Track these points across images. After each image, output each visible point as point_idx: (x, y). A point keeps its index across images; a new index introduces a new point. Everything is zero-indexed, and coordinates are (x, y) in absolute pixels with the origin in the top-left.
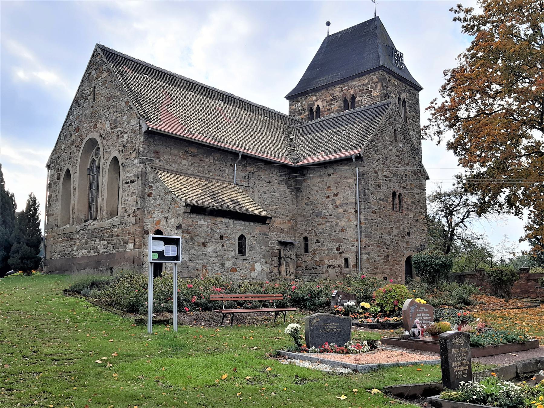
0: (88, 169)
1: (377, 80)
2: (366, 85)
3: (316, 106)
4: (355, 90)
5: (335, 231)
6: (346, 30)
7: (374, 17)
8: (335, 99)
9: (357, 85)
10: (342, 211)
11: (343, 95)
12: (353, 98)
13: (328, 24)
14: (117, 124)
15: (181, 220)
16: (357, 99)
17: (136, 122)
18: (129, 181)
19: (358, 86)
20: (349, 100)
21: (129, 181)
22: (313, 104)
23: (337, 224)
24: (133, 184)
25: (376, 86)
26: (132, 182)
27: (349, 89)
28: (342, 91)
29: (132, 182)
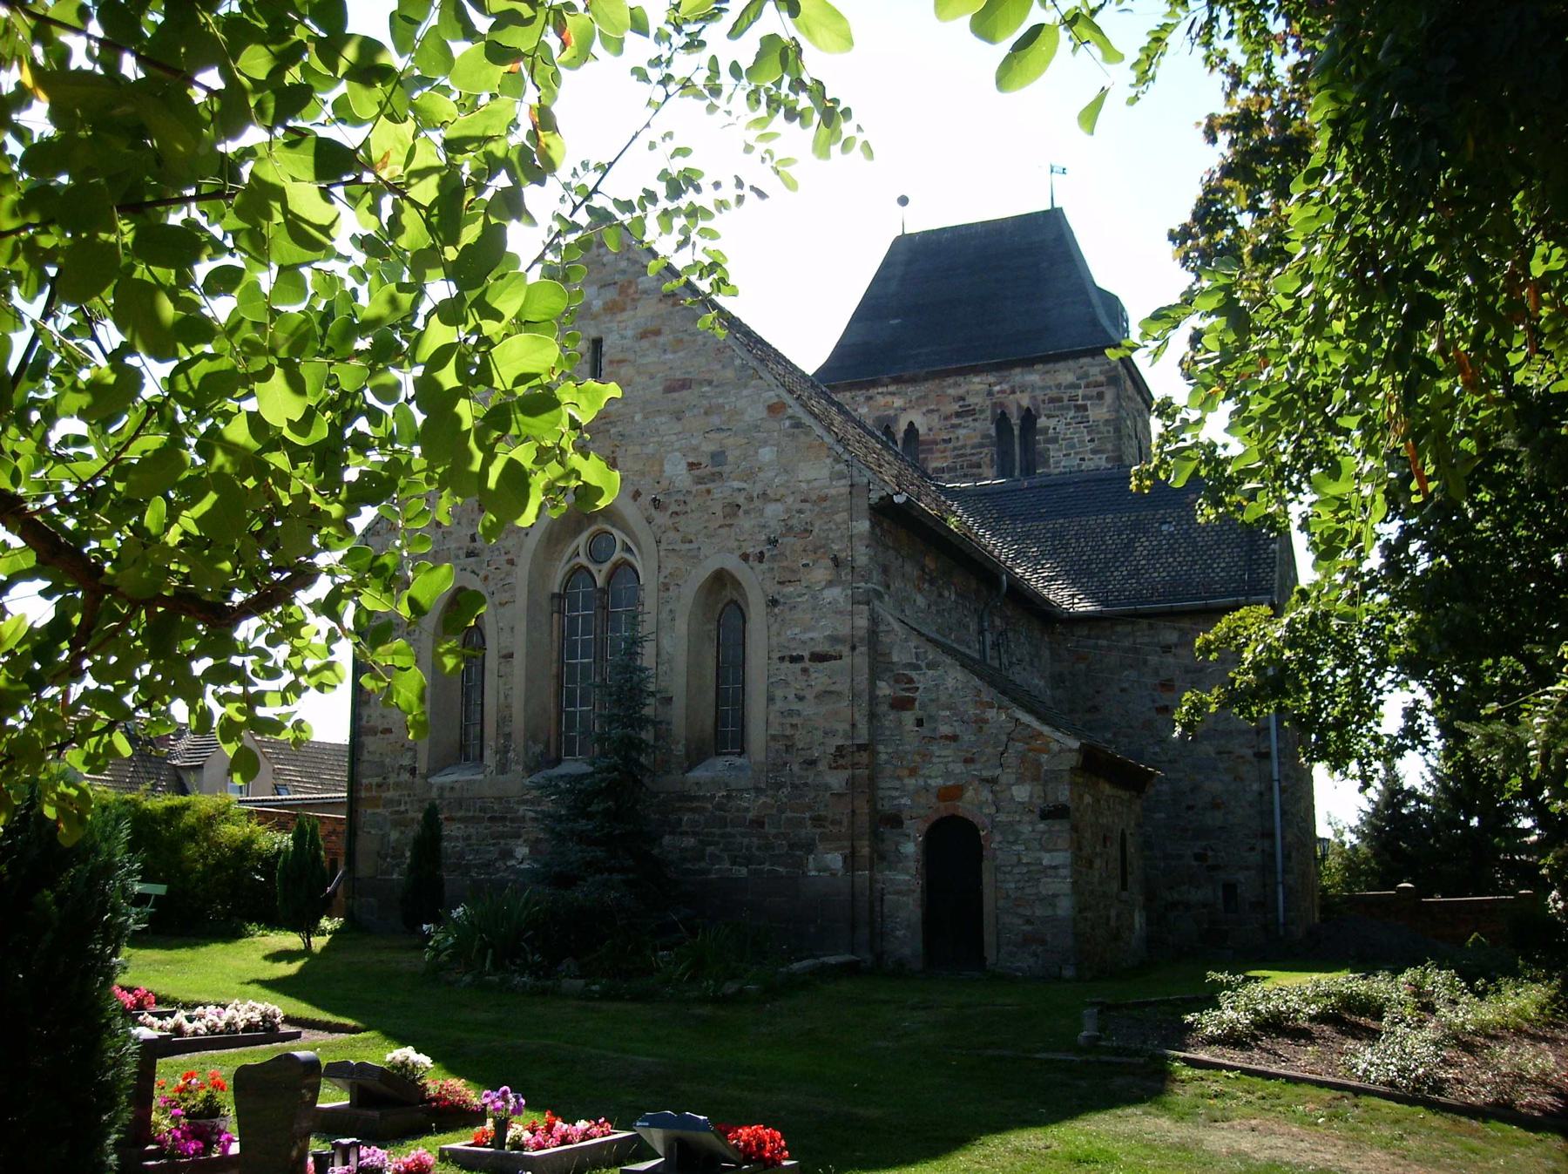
0: (554, 596)
1: (1102, 378)
2: (1067, 387)
3: (903, 426)
4: (1034, 398)
5: (1190, 808)
6: (983, 223)
7: (1048, 207)
8: (967, 412)
9: (1040, 384)
10: (1211, 751)
11: (995, 405)
12: (1029, 417)
13: (903, 201)
14: (727, 469)
15: (1063, 794)
16: (1042, 422)
17: (826, 472)
18: (806, 654)
19: (1043, 388)
20: (1015, 421)
21: (806, 654)
22: (895, 419)
23: (1195, 789)
24: (820, 666)
25: (1100, 396)
26: (818, 658)
27: (1013, 392)
28: (990, 394)
29: (818, 658)
